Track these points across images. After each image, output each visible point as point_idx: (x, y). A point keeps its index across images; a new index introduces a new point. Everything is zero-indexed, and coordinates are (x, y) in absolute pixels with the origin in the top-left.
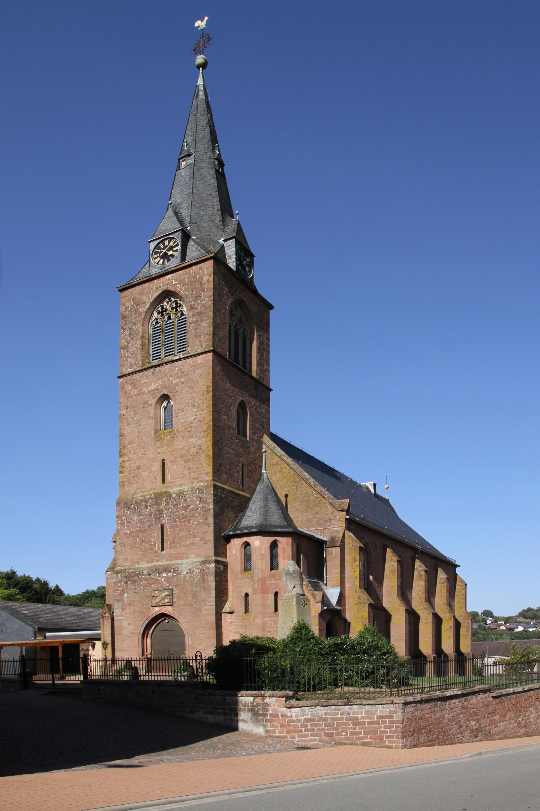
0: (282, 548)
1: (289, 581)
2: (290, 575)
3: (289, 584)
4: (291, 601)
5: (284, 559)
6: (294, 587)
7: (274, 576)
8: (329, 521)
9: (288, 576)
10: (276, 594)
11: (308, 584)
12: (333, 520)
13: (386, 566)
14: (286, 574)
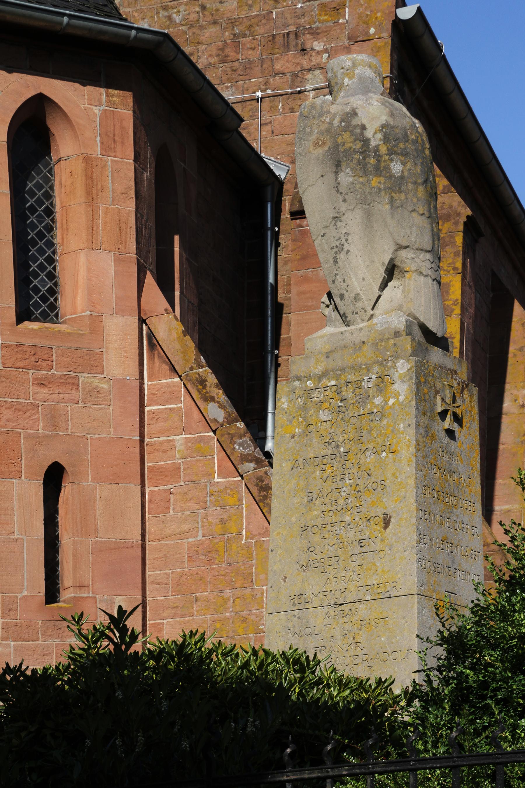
0: (78, 167)
1: (353, 220)
2: (363, 168)
3: (355, 245)
4: (369, 383)
5: (92, 246)
6: (391, 271)
7: (39, 357)
8: (294, 40)
9: (346, 178)
10: (54, 477)
11: (230, 421)
12: (315, 34)
13: (507, 405)
14: (337, 160)
